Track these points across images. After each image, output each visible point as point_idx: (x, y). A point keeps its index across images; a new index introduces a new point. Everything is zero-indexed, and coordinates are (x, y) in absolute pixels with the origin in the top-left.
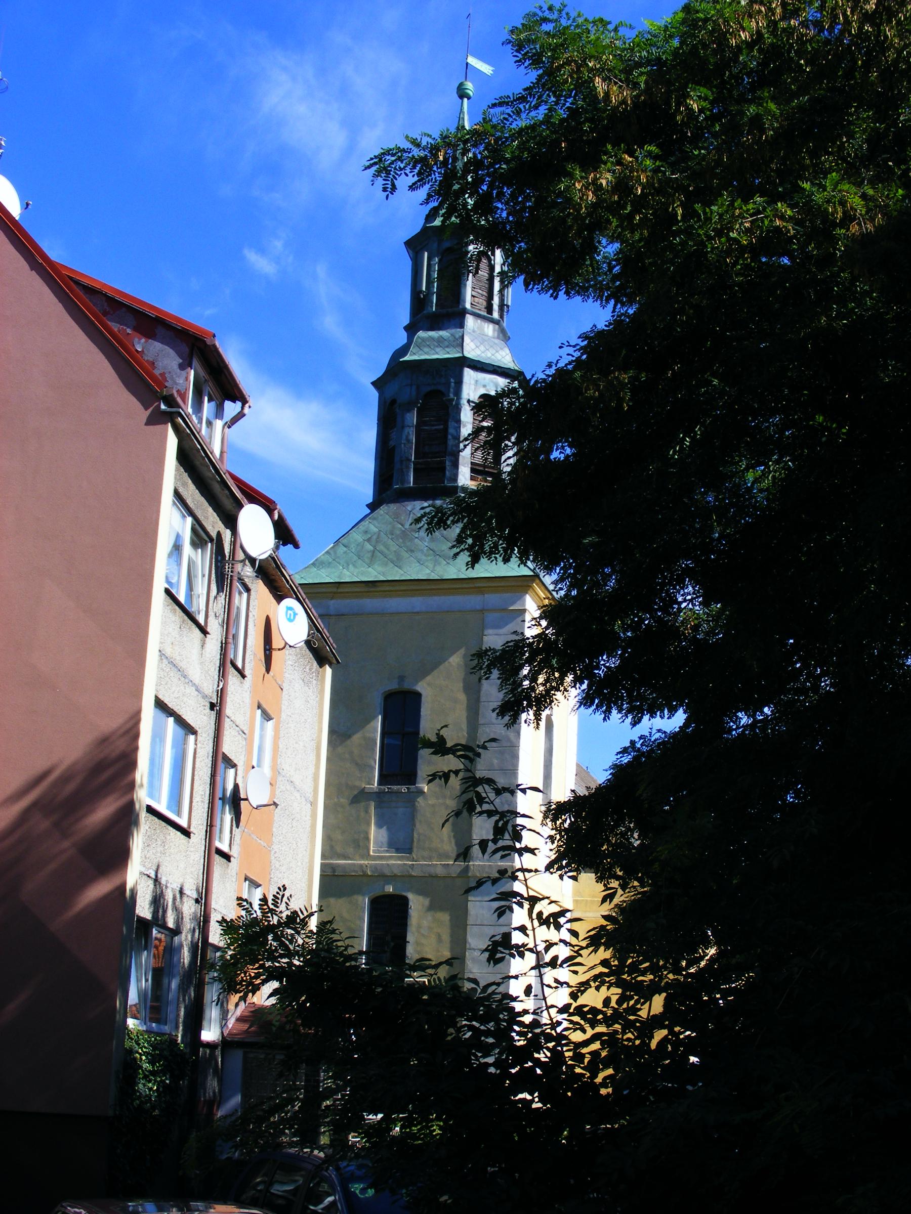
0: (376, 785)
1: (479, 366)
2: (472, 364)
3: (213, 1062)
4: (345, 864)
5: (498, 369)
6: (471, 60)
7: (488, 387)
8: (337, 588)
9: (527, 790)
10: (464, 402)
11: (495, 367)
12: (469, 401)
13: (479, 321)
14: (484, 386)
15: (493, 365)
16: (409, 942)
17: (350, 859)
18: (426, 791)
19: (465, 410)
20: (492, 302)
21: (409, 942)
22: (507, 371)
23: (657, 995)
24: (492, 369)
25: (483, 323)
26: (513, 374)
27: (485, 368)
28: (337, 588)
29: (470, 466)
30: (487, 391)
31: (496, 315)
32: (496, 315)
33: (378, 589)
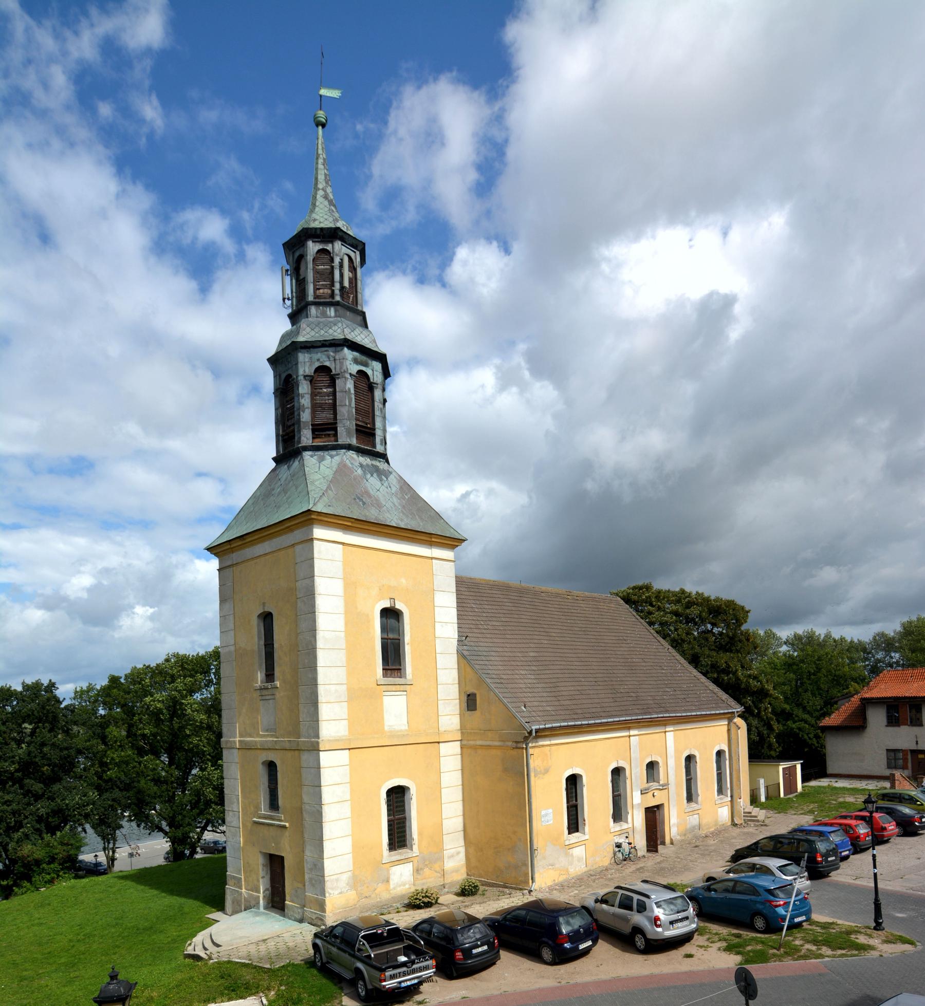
0: (259, 683)
1: (309, 345)
2: (303, 345)
3: (167, 829)
4: (251, 741)
5: (325, 343)
6: (323, 92)
7: (321, 360)
8: (230, 545)
9: (872, 928)
10: (301, 378)
11: (322, 342)
12: (305, 376)
13: (321, 308)
14: (318, 360)
15: (320, 341)
16: (50, 680)
17: (253, 737)
18: (278, 686)
19: (302, 384)
20: (712, 598)
21: (50, 680)
22: (332, 342)
23: (66, 692)
24: (320, 345)
25: (325, 309)
26: (339, 343)
27: (315, 345)
28: (230, 545)
29: (311, 427)
30: (322, 362)
31: (338, 298)
32: (338, 298)
33: (247, 540)
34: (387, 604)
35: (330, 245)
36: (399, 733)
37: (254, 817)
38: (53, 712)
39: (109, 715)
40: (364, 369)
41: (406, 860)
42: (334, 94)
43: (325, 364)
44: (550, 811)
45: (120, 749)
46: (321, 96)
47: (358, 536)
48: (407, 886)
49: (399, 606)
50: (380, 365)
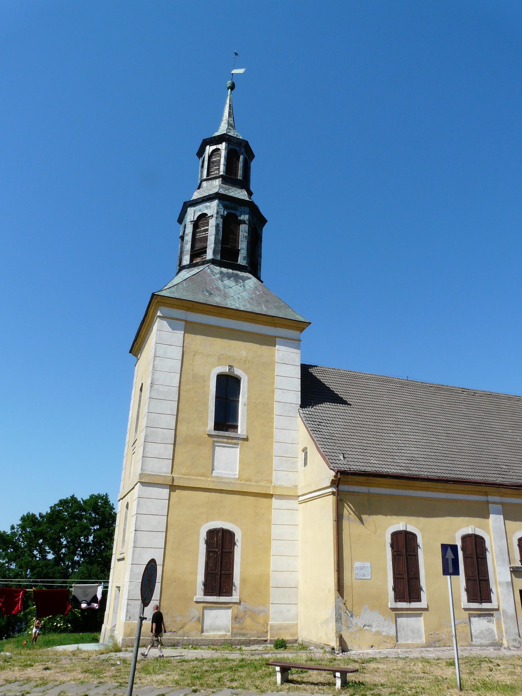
5: (204, 198)
6: (234, 71)
11: (202, 198)
15: (201, 198)
34: (225, 369)
35: (221, 145)
36: (226, 481)
37: (276, 683)
38: (23, 647)
39: (60, 625)
40: (233, 212)
41: (226, 605)
42: (241, 71)
43: (204, 212)
44: (368, 564)
45: (125, 661)
46: (232, 74)
47: (335, 585)
48: (222, 633)
49: (238, 372)
50: (248, 209)
